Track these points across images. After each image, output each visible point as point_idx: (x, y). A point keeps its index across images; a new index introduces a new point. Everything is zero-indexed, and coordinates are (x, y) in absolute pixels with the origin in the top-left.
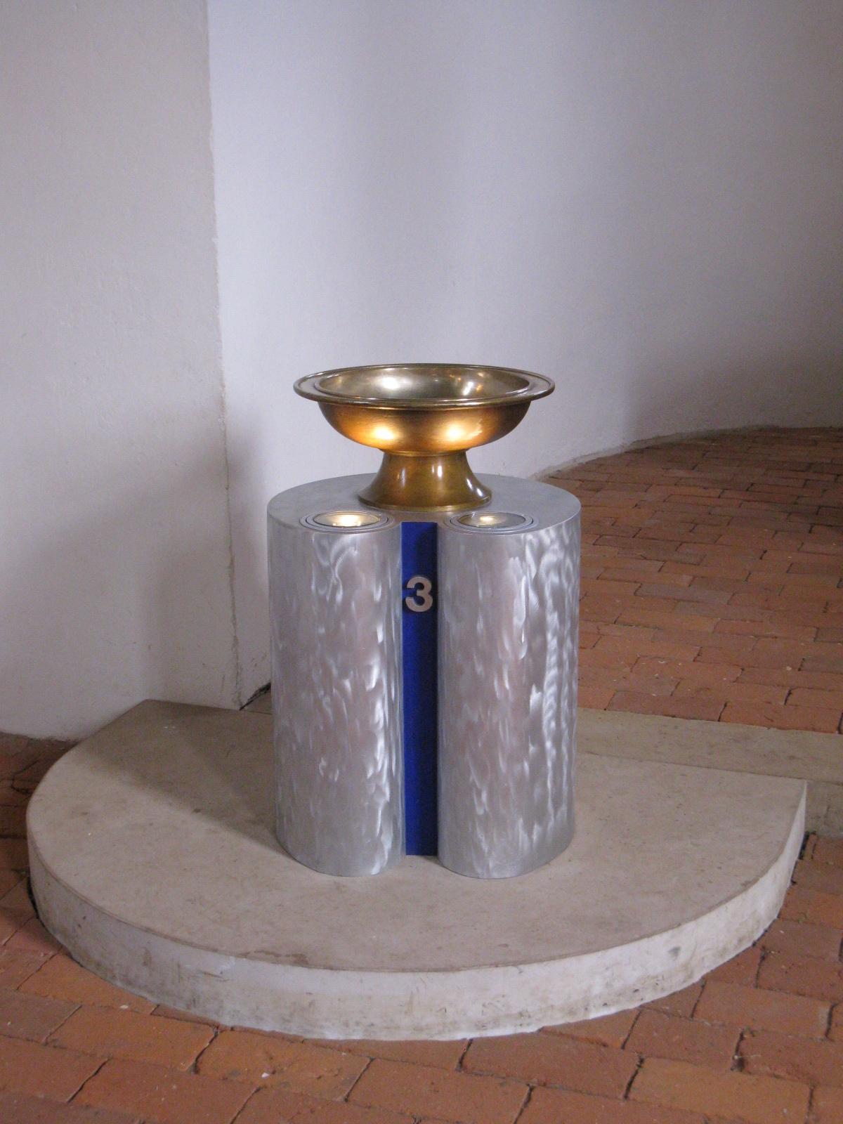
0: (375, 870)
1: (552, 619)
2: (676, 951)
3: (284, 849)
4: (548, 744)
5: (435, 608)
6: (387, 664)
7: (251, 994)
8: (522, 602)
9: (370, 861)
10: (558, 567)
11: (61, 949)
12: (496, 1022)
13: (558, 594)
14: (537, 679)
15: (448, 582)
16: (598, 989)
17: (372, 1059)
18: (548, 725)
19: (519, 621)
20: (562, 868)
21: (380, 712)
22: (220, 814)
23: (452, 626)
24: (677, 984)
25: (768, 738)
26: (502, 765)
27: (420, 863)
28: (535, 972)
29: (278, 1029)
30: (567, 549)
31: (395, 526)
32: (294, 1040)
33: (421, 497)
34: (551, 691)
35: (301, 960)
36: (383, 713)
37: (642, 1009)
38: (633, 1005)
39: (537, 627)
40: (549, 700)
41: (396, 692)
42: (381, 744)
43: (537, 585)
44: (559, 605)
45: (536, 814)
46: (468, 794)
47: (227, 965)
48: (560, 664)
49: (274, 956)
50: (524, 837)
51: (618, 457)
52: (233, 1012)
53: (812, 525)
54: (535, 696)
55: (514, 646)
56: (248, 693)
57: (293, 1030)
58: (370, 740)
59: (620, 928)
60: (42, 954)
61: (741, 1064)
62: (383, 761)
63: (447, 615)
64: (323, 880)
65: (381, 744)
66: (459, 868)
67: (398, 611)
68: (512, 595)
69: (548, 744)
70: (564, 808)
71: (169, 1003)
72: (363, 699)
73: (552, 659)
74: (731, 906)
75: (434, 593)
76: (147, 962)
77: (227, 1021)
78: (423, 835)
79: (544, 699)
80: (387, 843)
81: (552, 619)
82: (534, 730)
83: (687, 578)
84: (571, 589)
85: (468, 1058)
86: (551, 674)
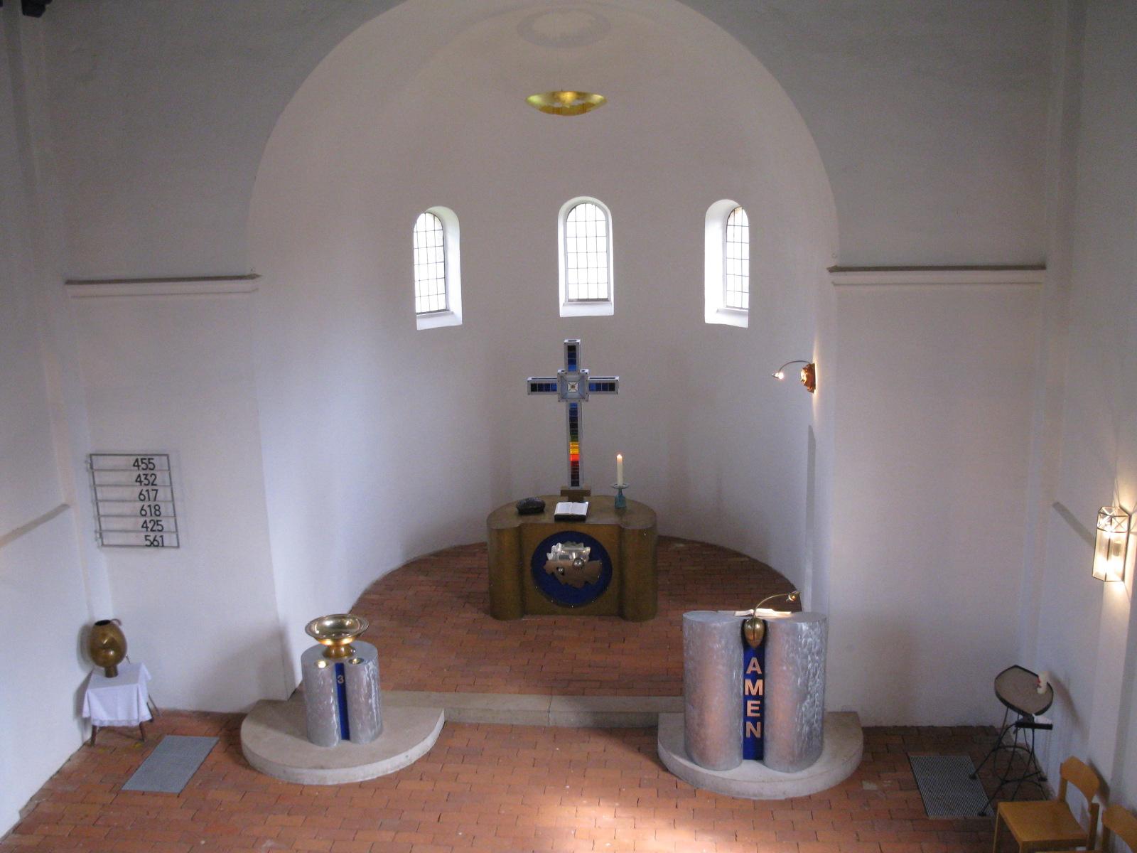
0: (335, 745)
1: (373, 682)
2: (407, 756)
3: (312, 742)
4: (374, 711)
5: (344, 683)
6: (334, 698)
7: (310, 777)
8: (365, 678)
9: (334, 743)
10: (373, 670)
11: (259, 772)
12: (367, 777)
13: (374, 676)
14: (370, 696)
15: (347, 678)
16: (389, 767)
17: (340, 788)
18: (374, 706)
19: (365, 684)
20: (379, 740)
21: (334, 708)
22: (292, 734)
23: (349, 688)
24: (409, 764)
25: (435, 695)
26: (364, 717)
27: (346, 743)
28: (375, 765)
29: (318, 784)
30: (375, 665)
31: (333, 664)
32: (321, 786)
33: (338, 655)
34: (374, 698)
35: (322, 768)
36: (334, 708)
37: (400, 770)
38: (398, 769)
39: (369, 685)
40: (373, 702)
41: (337, 703)
42: (334, 715)
43: (369, 676)
44: (374, 678)
45: (373, 727)
46: (356, 725)
47: (305, 771)
48: (375, 691)
49: (316, 768)
50: (370, 733)
51: (398, 570)
52: (307, 781)
53: (465, 603)
54: (370, 701)
55: (364, 690)
56: (290, 695)
57: (322, 783)
58: (331, 714)
59: (393, 753)
60: (255, 774)
61: (421, 779)
62: (335, 719)
63: (347, 683)
64: (323, 748)
65: (334, 715)
66: (355, 742)
67: (336, 685)
68: (362, 679)
69: (374, 711)
70: (380, 724)
71: (291, 781)
72: (330, 706)
73: (373, 691)
74: (421, 744)
75: (344, 678)
76: (285, 772)
77: (305, 783)
78: (346, 734)
79: (373, 701)
80: (337, 738)
81: (373, 682)
82: (371, 709)
83: (419, 635)
84: (377, 676)
85: (361, 785)
86: (373, 694)
